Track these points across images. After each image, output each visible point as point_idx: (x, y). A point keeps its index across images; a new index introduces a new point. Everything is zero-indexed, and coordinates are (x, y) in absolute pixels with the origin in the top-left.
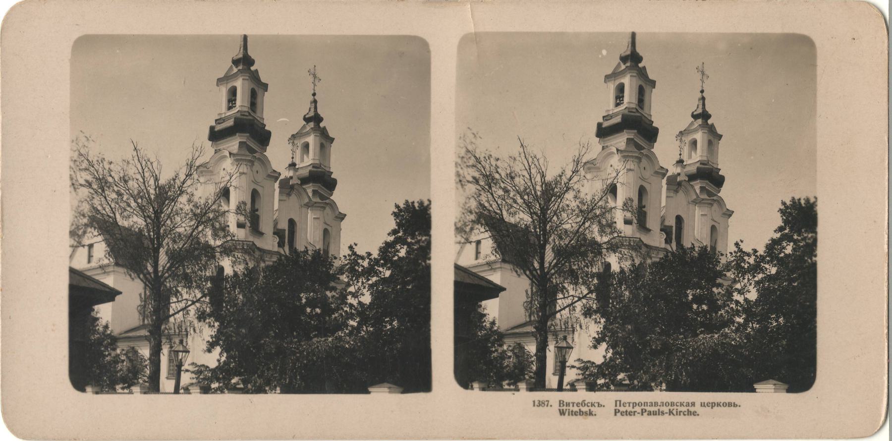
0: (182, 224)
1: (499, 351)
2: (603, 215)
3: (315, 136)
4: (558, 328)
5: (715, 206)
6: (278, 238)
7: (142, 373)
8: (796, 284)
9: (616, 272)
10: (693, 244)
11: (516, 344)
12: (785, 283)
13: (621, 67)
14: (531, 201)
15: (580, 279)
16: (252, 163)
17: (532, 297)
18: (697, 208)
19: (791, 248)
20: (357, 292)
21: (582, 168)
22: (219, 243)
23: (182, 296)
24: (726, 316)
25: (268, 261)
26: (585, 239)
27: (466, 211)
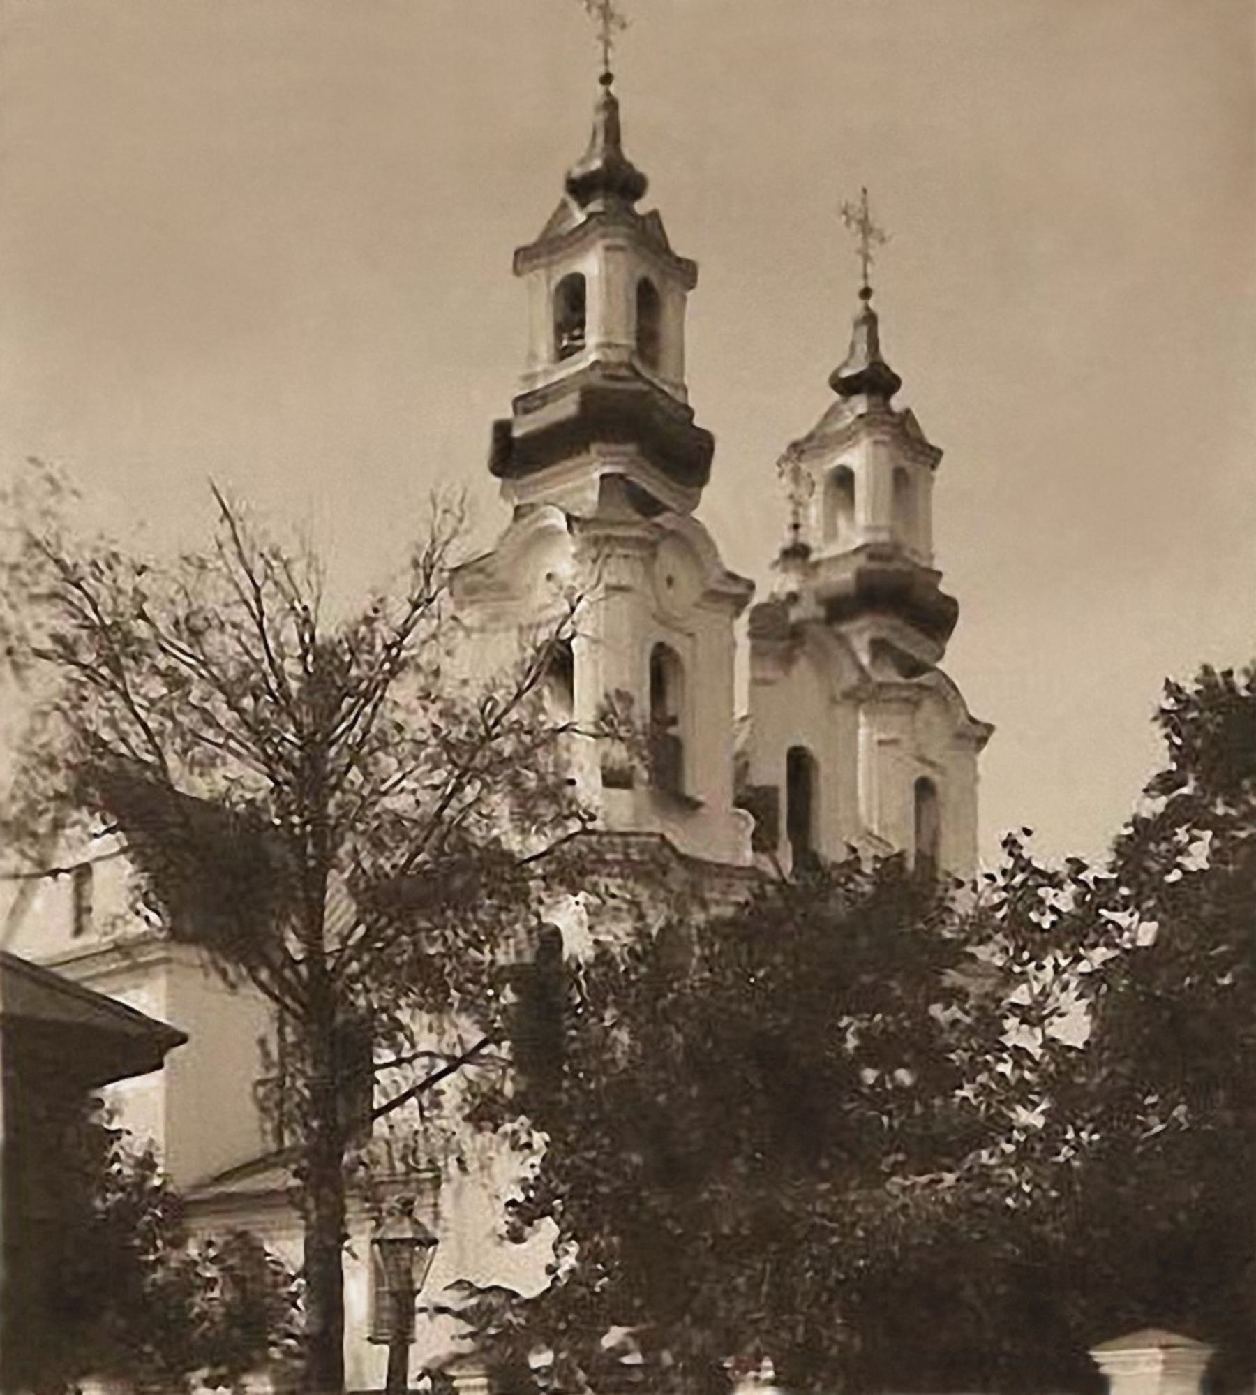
0: (404, 783)
1: (173, 1264)
2: (525, 755)
3: (876, 443)
4: (381, 1171)
5: (928, 707)
6: (751, 819)
7: (282, 1325)
8: (1226, 981)
9: (581, 961)
10: (853, 850)
11: (230, 1238)
12: (1188, 981)
13: (571, 216)
14: (268, 715)
15: (453, 992)
16: (650, 548)
17: (282, 1065)
18: (862, 718)
19: (1207, 852)
20: (1038, 1004)
21: (445, 590)
22: (538, 844)
23: (413, 1046)
24: (983, 1107)
25: (717, 903)
26: (465, 846)
27: (34, 761)
